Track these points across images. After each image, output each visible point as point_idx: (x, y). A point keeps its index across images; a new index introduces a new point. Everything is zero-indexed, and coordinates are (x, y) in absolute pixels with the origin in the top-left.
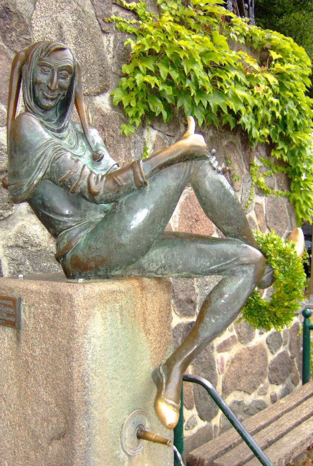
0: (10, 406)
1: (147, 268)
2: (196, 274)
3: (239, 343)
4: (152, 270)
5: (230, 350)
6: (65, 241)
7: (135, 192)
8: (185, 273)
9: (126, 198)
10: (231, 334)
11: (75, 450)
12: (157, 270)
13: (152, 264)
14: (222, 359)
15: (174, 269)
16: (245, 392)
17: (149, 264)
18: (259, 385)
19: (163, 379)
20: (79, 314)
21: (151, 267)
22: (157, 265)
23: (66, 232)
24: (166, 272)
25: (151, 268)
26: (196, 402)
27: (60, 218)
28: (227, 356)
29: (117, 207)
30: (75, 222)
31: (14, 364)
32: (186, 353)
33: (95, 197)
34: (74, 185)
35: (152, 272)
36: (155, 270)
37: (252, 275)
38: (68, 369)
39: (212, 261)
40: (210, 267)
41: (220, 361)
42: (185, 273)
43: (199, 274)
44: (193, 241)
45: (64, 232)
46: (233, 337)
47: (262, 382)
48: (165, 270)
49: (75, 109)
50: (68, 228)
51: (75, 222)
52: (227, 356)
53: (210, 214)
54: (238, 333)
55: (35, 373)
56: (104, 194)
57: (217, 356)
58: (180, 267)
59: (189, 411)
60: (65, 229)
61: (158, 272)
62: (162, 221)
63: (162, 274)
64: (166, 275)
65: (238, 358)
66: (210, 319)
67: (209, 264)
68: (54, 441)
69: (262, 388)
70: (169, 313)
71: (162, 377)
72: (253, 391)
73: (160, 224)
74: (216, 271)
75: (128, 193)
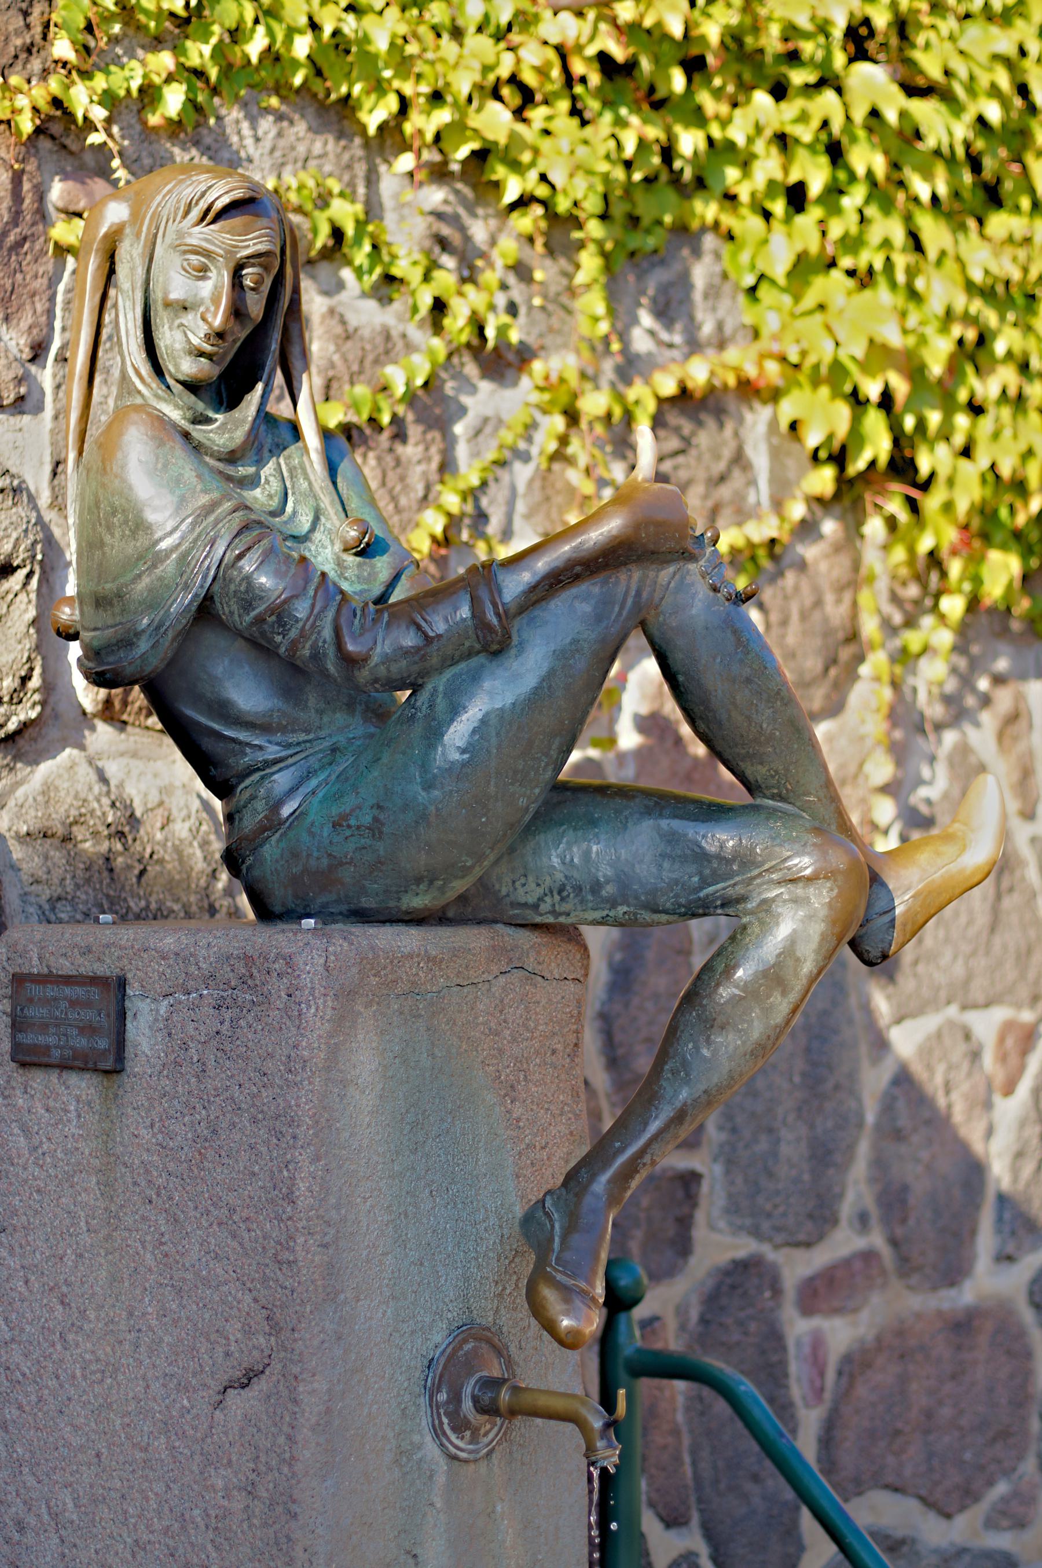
0: (83, 1313)
1: (508, 895)
2: (660, 912)
3: (896, 1284)
4: (522, 900)
5: (855, 1310)
6: (260, 805)
7: (474, 662)
8: (625, 909)
9: (448, 674)
10: (860, 1243)
11: (295, 1402)
12: (541, 899)
13: (523, 880)
14: (817, 1343)
15: (590, 897)
16: (923, 1500)
17: (514, 882)
18: (990, 1483)
19: (553, 1227)
20: (313, 1011)
21: (521, 891)
22: (538, 885)
23: (262, 778)
24: (565, 907)
25: (521, 896)
26: (700, 1501)
27: (242, 736)
28: (840, 1334)
29: (419, 704)
30: (289, 746)
31: (98, 1183)
32: (621, 1150)
33: (356, 673)
34: (293, 634)
35: (525, 905)
36: (531, 900)
37: (823, 913)
38: (281, 1171)
39: (707, 872)
40: (701, 889)
41: (807, 1350)
42: (625, 909)
43: (666, 912)
44: (648, 812)
45: (256, 776)
46: (869, 1256)
47: (1008, 1472)
48: (562, 899)
49: (279, 378)
50: (268, 767)
51: (289, 746)
52: (840, 1334)
53: (702, 727)
54: (894, 1242)
55: (171, 1198)
56: (383, 663)
57: (798, 1327)
58: (609, 890)
59: (672, 1535)
60: (258, 769)
61: (544, 907)
62: (554, 747)
63: (553, 912)
64: (568, 914)
65: (896, 1344)
66: (697, 1048)
67: (696, 879)
68: (231, 1392)
69: (1004, 1500)
70: (576, 1045)
71: (551, 1220)
72: (963, 1508)
73: (547, 755)
74: (719, 903)
75: (454, 662)
